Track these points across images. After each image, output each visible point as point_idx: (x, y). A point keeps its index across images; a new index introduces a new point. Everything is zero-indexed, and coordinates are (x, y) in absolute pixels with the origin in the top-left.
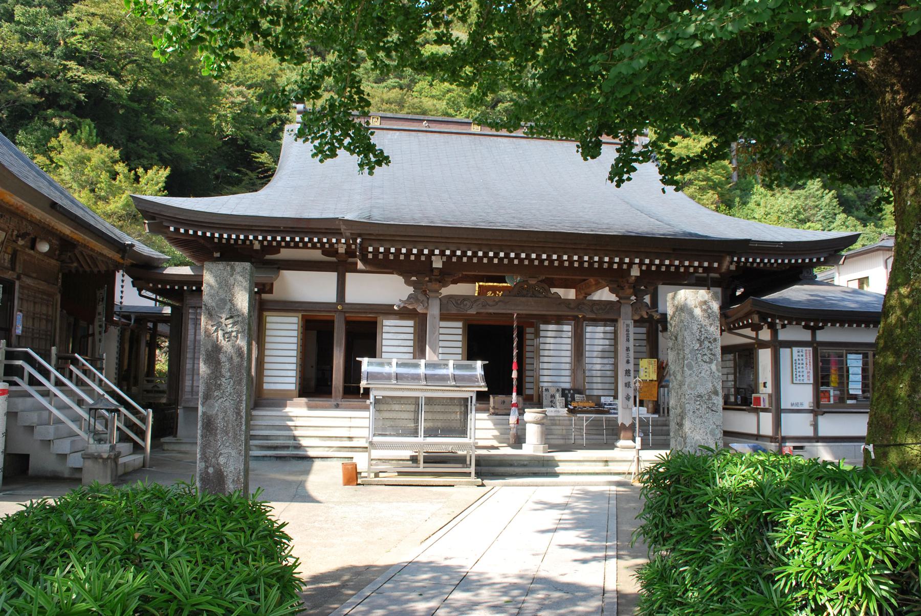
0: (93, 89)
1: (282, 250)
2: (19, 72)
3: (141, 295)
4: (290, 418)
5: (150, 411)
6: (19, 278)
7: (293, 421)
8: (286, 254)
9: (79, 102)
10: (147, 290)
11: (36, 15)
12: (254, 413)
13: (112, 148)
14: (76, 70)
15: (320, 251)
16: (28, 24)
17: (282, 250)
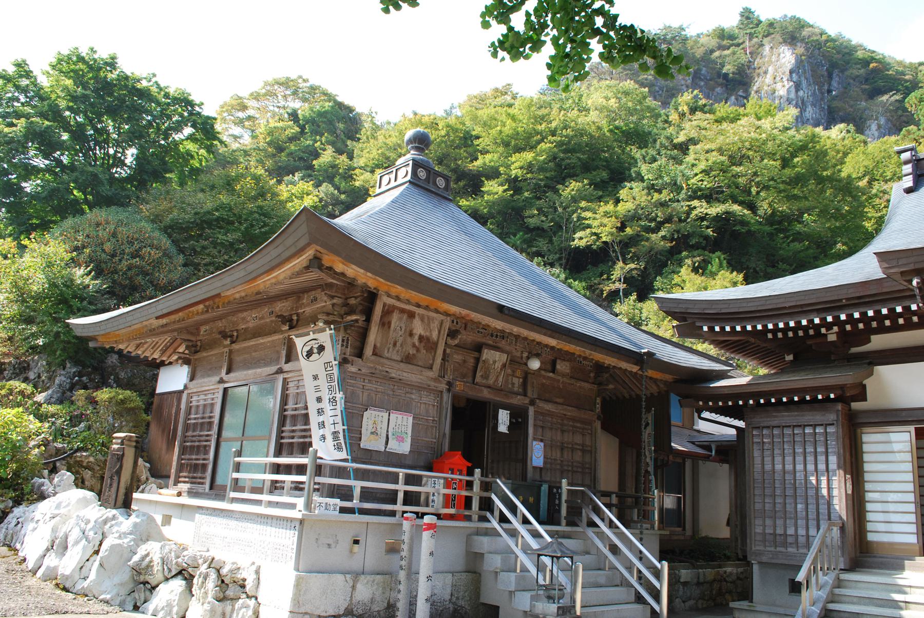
0: (723, 222)
1: (873, 337)
2: (653, 225)
4: (900, 590)
5: (665, 564)
6: (532, 403)
7: (905, 593)
8: (879, 342)
9: (706, 238)
11: (659, 169)
13: (735, 273)
14: (701, 208)
16: (657, 179)
17: (873, 337)
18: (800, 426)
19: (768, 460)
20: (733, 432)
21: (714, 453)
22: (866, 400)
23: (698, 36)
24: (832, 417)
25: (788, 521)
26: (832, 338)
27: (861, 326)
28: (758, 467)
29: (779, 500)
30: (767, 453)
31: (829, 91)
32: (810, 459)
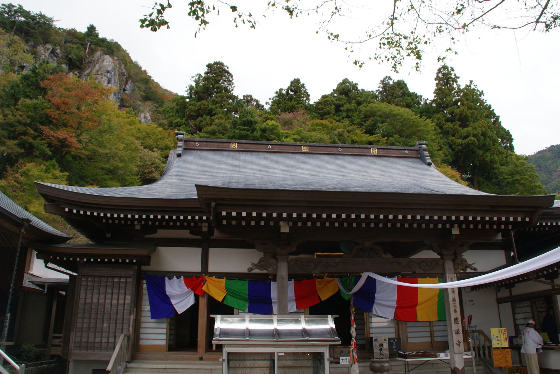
1: (159, 231)
3: (46, 267)
8: (161, 233)
10: (52, 263)
12: (130, 365)
15: (188, 231)
17: (159, 231)
18: (112, 277)
19: (89, 296)
20: (67, 277)
21: (46, 290)
22: (149, 265)
23: (60, 29)
24: (131, 273)
25: (97, 334)
26: (138, 227)
27: (354, 225)
28: (82, 300)
29: (93, 321)
30: (89, 292)
31: (124, 90)
32: (115, 296)
